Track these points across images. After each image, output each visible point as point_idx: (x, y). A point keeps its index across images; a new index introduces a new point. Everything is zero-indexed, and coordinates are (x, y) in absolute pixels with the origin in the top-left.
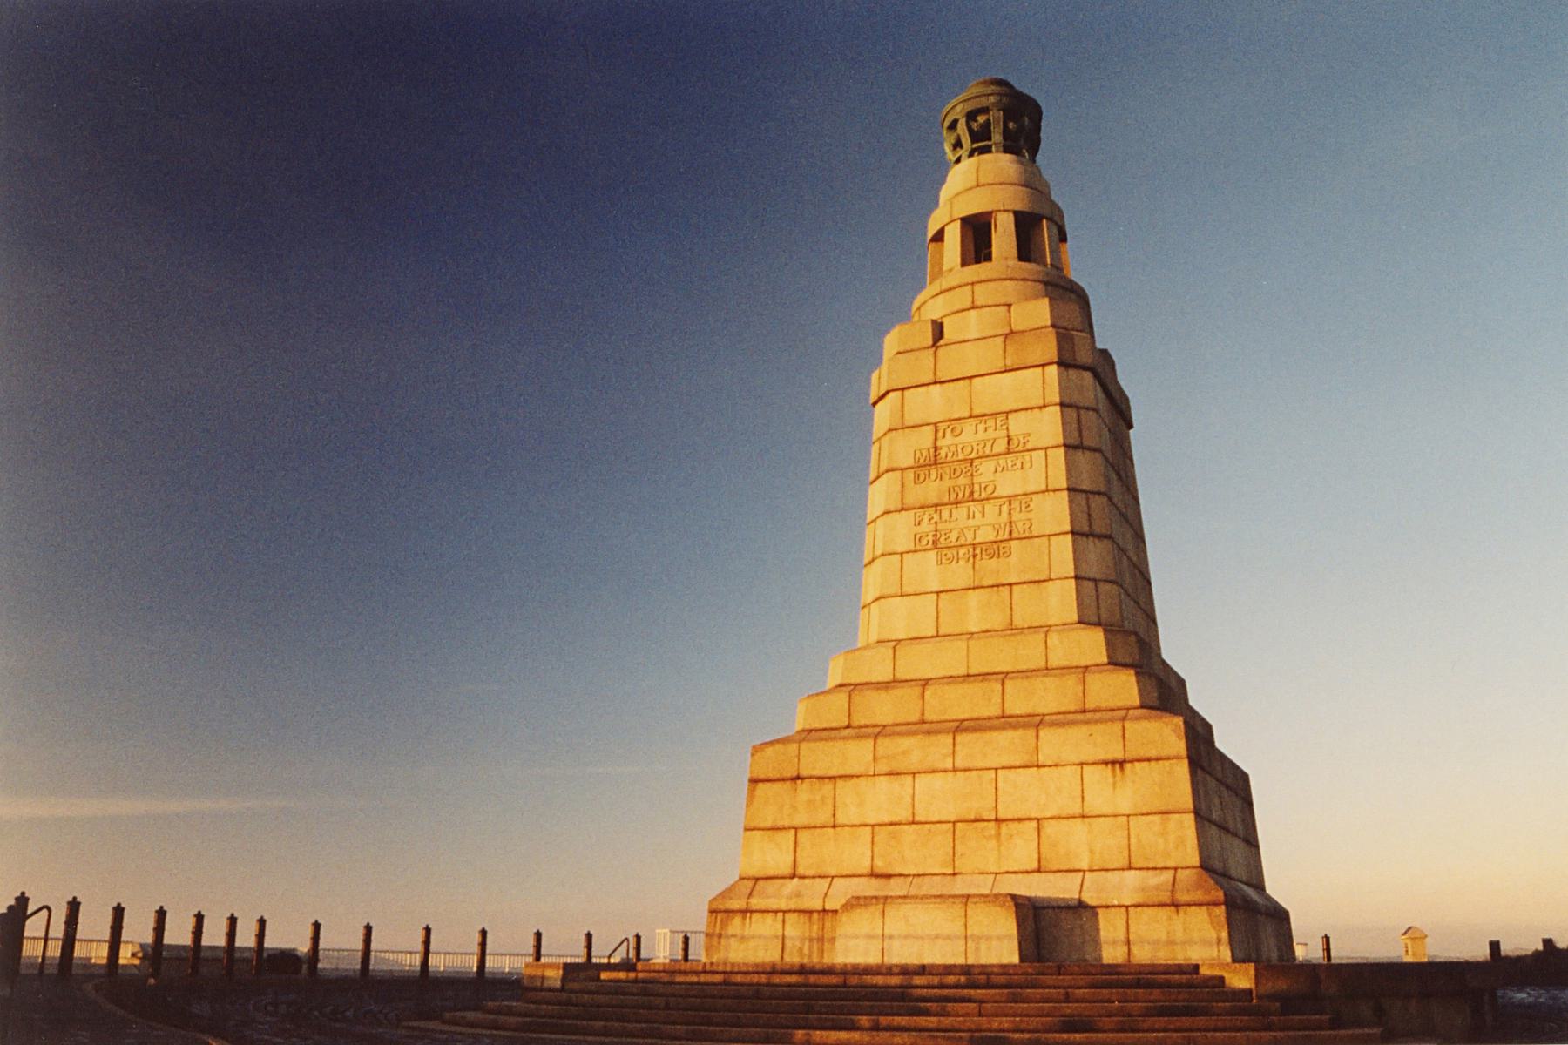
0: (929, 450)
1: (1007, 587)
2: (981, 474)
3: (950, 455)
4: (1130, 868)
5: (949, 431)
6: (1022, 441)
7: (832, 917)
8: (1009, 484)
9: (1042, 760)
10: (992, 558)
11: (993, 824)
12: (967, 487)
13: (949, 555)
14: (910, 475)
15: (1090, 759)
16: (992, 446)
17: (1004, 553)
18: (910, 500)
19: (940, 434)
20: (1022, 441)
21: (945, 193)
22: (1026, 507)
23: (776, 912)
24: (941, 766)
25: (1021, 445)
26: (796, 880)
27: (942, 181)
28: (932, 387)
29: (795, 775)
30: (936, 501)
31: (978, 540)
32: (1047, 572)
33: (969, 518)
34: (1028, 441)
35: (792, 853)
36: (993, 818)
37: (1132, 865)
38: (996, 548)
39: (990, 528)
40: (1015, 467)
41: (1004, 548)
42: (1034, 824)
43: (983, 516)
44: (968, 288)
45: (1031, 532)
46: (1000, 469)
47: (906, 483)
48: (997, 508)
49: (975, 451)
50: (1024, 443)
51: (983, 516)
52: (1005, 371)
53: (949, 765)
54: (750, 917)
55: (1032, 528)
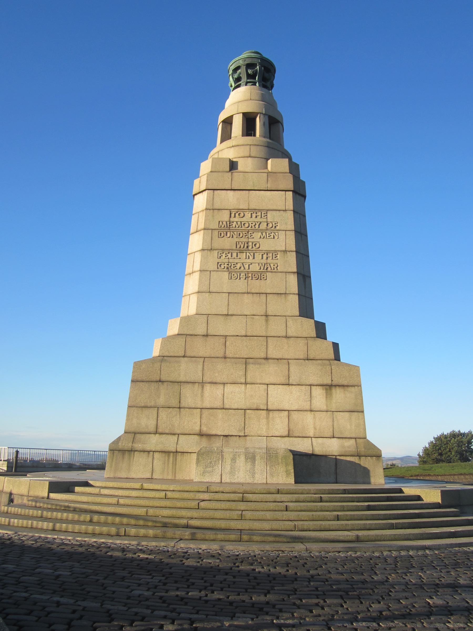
0: (227, 223)
1: (265, 294)
2: (253, 238)
3: (237, 226)
4: (334, 437)
5: (237, 215)
6: (274, 225)
7: (181, 455)
8: (267, 245)
9: (291, 382)
10: (258, 279)
11: (264, 412)
12: (246, 243)
13: (236, 275)
14: (216, 233)
15: (315, 383)
16: (259, 225)
17: (263, 278)
18: (215, 245)
19: (233, 215)
20: (274, 225)
21: (228, 103)
22: (275, 257)
23: (149, 452)
24: (239, 381)
25: (274, 227)
26: (157, 435)
27: (228, 97)
28: (229, 192)
29: (158, 379)
30: (229, 248)
31: (250, 270)
32: (285, 290)
33: (246, 258)
34: (277, 226)
35: (156, 421)
36: (266, 408)
37: (334, 435)
38: (259, 276)
39: (257, 264)
40: (270, 237)
41: (263, 275)
42: (286, 413)
43: (254, 258)
44: (249, 146)
45: (277, 270)
46: (262, 237)
47: (213, 237)
48: (261, 256)
49: (250, 227)
50: (275, 227)
51: (254, 258)
52: (267, 190)
53: (243, 381)
54: (134, 454)
55: (278, 268)
